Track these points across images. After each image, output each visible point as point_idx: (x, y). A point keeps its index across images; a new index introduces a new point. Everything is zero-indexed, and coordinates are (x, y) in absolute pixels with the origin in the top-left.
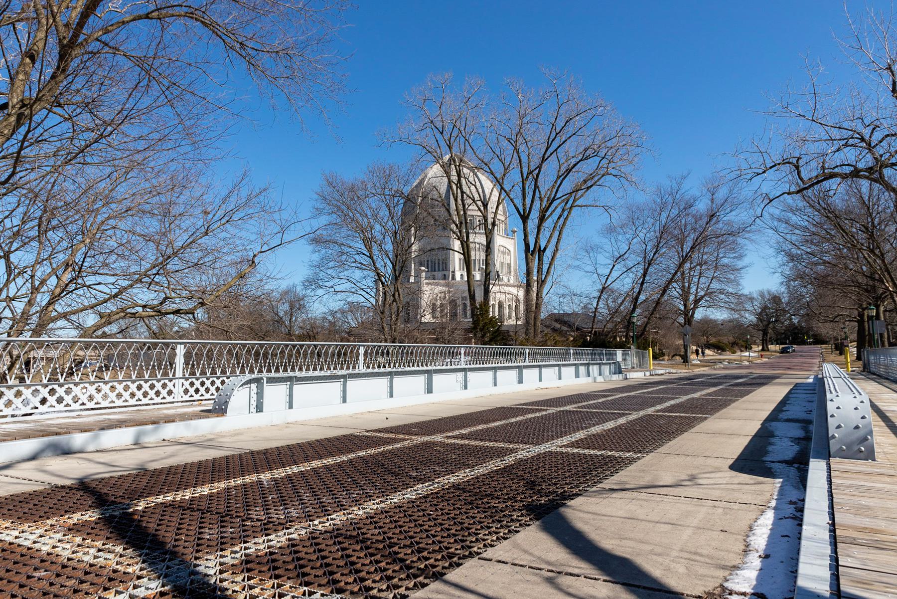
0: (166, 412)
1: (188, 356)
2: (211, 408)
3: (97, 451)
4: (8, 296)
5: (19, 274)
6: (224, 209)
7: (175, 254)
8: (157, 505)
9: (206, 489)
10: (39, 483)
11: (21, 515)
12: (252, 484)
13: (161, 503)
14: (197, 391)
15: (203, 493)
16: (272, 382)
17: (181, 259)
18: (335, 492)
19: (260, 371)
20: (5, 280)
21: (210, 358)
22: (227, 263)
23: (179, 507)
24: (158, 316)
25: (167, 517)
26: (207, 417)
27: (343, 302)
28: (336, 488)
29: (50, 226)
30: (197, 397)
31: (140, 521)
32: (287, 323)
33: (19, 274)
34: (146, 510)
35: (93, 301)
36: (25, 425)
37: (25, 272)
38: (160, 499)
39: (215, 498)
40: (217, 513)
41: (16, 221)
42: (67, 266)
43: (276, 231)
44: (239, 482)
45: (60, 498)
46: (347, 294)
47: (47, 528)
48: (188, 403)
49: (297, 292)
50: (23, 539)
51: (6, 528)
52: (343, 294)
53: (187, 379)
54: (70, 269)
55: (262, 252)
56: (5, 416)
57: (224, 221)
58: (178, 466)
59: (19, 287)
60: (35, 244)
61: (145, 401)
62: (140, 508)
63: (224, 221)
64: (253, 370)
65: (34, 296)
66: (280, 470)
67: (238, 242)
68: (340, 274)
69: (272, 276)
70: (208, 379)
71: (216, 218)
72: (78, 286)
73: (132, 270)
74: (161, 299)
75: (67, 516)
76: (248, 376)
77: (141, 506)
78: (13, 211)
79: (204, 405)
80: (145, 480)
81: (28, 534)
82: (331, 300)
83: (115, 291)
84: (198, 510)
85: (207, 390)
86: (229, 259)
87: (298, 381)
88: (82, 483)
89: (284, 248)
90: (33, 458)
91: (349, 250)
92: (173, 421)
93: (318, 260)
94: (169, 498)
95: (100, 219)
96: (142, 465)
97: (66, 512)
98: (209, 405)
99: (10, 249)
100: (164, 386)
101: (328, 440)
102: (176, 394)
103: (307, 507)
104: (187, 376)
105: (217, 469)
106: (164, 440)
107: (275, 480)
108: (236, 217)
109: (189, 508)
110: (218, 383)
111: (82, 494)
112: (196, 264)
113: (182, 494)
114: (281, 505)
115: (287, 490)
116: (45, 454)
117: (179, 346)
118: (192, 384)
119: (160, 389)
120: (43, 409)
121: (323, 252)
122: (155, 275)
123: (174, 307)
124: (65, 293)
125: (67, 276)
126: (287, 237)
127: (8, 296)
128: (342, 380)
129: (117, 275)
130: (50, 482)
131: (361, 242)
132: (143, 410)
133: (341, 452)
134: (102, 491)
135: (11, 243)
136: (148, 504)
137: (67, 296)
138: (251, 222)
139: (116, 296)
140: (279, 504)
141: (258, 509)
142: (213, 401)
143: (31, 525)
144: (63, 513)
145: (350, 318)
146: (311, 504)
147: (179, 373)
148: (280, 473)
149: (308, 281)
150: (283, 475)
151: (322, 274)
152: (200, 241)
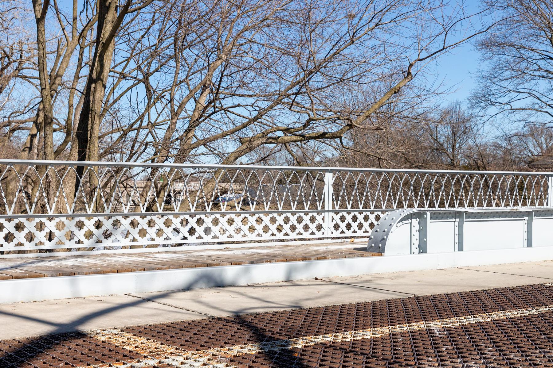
0: (316, 248)
1: (337, 185)
2: (366, 246)
3: (249, 286)
4: (149, 122)
5: (158, 98)
6: (372, 9)
7: (317, 68)
8: (317, 344)
9: (368, 333)
10: (196, 313)
11: (183, 343)
12: (420, 332)
13: (321, 344)
14: (349, 226)
15: (365, 337)
16: (437, 218)
17: (323, 74)
18: (526, 349)
19: (421, 205)
20: (146, 104)
21: (521, 189)
22: (377, 77)
23: (341, 349)
24: (301, 141)
25: (329, 358)
26: (362, 256)
27: (523, 123)
28: (527, 345)
29: (185, 43)
30: (349, 233)
31: (301, 359)
32: (450, 151)
33: (158, 98)
34: (306, 349)
35: (231, 127)
36: (177, 255)
37: (163, 97)
38: (320, 339)
39: (380, 343)
40: (383, 359)
41: (153, 40)
42: (204, 87)
43: (437, 32)
44: (405, 329)
45: (218, 329)
46: (528, 112)
47: (210, 357)
48: (339, 240)
49: (462, 111)
50: (188, 365)
51: (171, 353)
52: (522, 112)
53: (337, 213)
54: (208, 91)
55: (419, 60)
56: (156, 246)
57: (372, 25)
58: (334, 307)
59: (159, 112)
60: (172, 63)
61: (293, 235)
62: (299, 347)
63: (372, 25)
64: (444, 204)
65: (174, 121)
66: (453, 319)
67: (390, 50)
68: (519, 87)
69: (432, 90)
70: (360, 213)
71: (362, 22)
72: (217, 109)
73: (271, 89)
74: (304, 122)
75: (227, 348)
76: (407, 211)
77: (300, 344)
78: (149, 29)
79: (358, 243)
80: (301, 318)
81: (192, 361)
82: (506, 121)
83: (255, 114)
84: (362, 354)
85: (360, 226)
86: (380, 71)
87: (469, 217)
88: (238, 316)
89: (448, 53)
90: (188, 288)
91: (531, 54)
92: (325, 258)
93: (489, 69)
94: (329, 339)
95: (235, 32)
96: (297, 303)
97: (225, 343)
98: (364, 243)
99: (148, 70)
100: (313, 220)
101: (511, 289)
102: (326, 229)
103: (491, 363)
104: (337, 209)
105: (378, 312)
106: (316, 279)
107: (448, 330)
108: (386, 19)
109: (351, 351)
110: (372, 218)
111: (239, 327)
112: (342, 80)
113: (342, 335)
114: (458, 357)
115: (464, 342)
116: (199, 285)
117: (327, 174)
118: (343, 219)
119: (309, 223)
120: (192, 239)
121: (495, 59)
122: (296, 94)
123: (320, 130)
124: (203, 118)
125: (204, 99)
126: (451, 39)
127: (149, 122)
128: (526, 218)
129: (255, 96)
130: (207, 313)
131: (548, 42)
132: (291, 246)
133: (528, 304)
134: (258, 326)
135: (150, 64)
136: (307, 343)
137: (206, 121)
138: (406, 23)
139: (255, 119)
140: (456, 356)
141: (430, 359)
142: (367, 239)
143: (194, 352)
144: (222, 344)
145: (530, 144)
146: (495, 360)
147: (328, 205)
148: (453, 323)
149: (476, 97)
150: (458, 325)
151: (494, 88)
152: (346, 52)
